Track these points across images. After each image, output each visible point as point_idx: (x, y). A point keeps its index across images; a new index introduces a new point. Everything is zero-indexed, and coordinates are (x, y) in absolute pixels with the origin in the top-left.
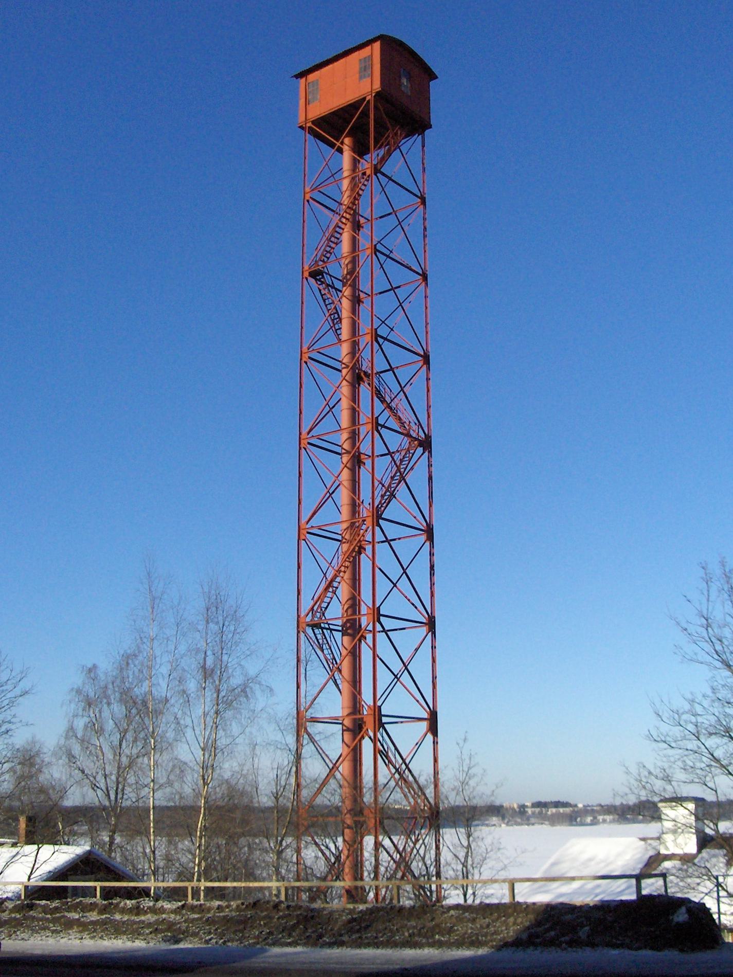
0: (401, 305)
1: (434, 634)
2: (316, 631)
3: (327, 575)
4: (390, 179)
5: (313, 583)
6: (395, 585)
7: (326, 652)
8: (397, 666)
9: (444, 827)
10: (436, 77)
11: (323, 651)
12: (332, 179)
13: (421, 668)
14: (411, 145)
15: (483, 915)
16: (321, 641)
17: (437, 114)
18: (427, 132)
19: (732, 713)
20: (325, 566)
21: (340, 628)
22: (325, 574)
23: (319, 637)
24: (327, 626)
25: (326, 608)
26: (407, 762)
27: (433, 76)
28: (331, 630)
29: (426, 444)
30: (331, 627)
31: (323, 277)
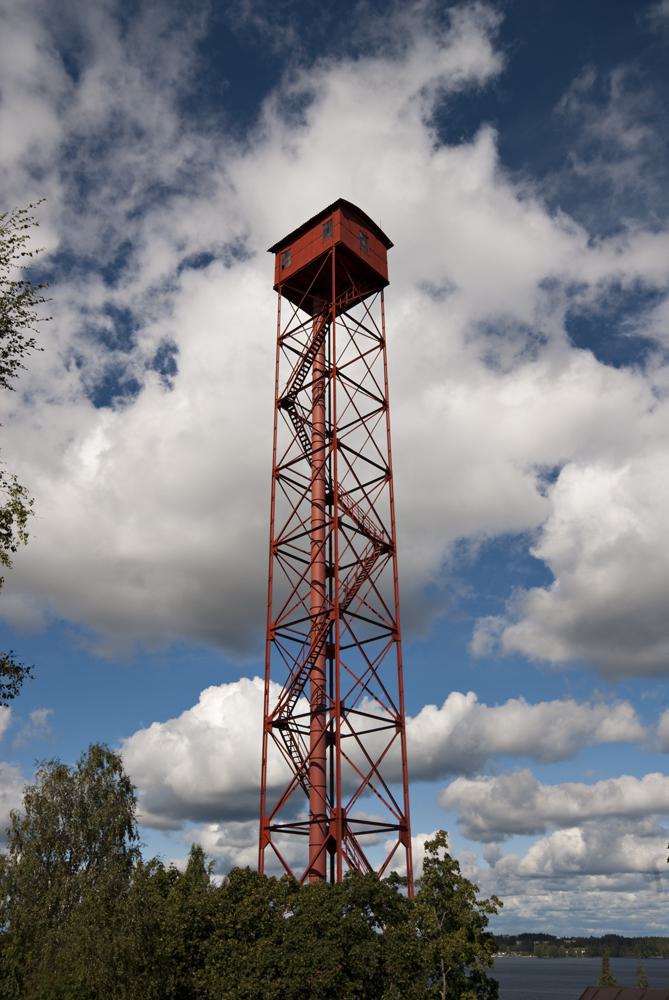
0: (359, 644)
2: (284, 732)
3: (294, 672)
7: (294, 755)
10: (392, 245)
12: (302, 329)
13: (387, 670)
14: (373, 300)
15: (645, 166)
16: (289, 744)
17: (392, 275)
18: (385, 289)
19: (666, 827)
21: (308, 731)
23: (287, 738)
24: (295, 728)
26: (374, 667)
27: (388, 244)
28: (300, 733)
30: (301, 729)
31: (294, 408)
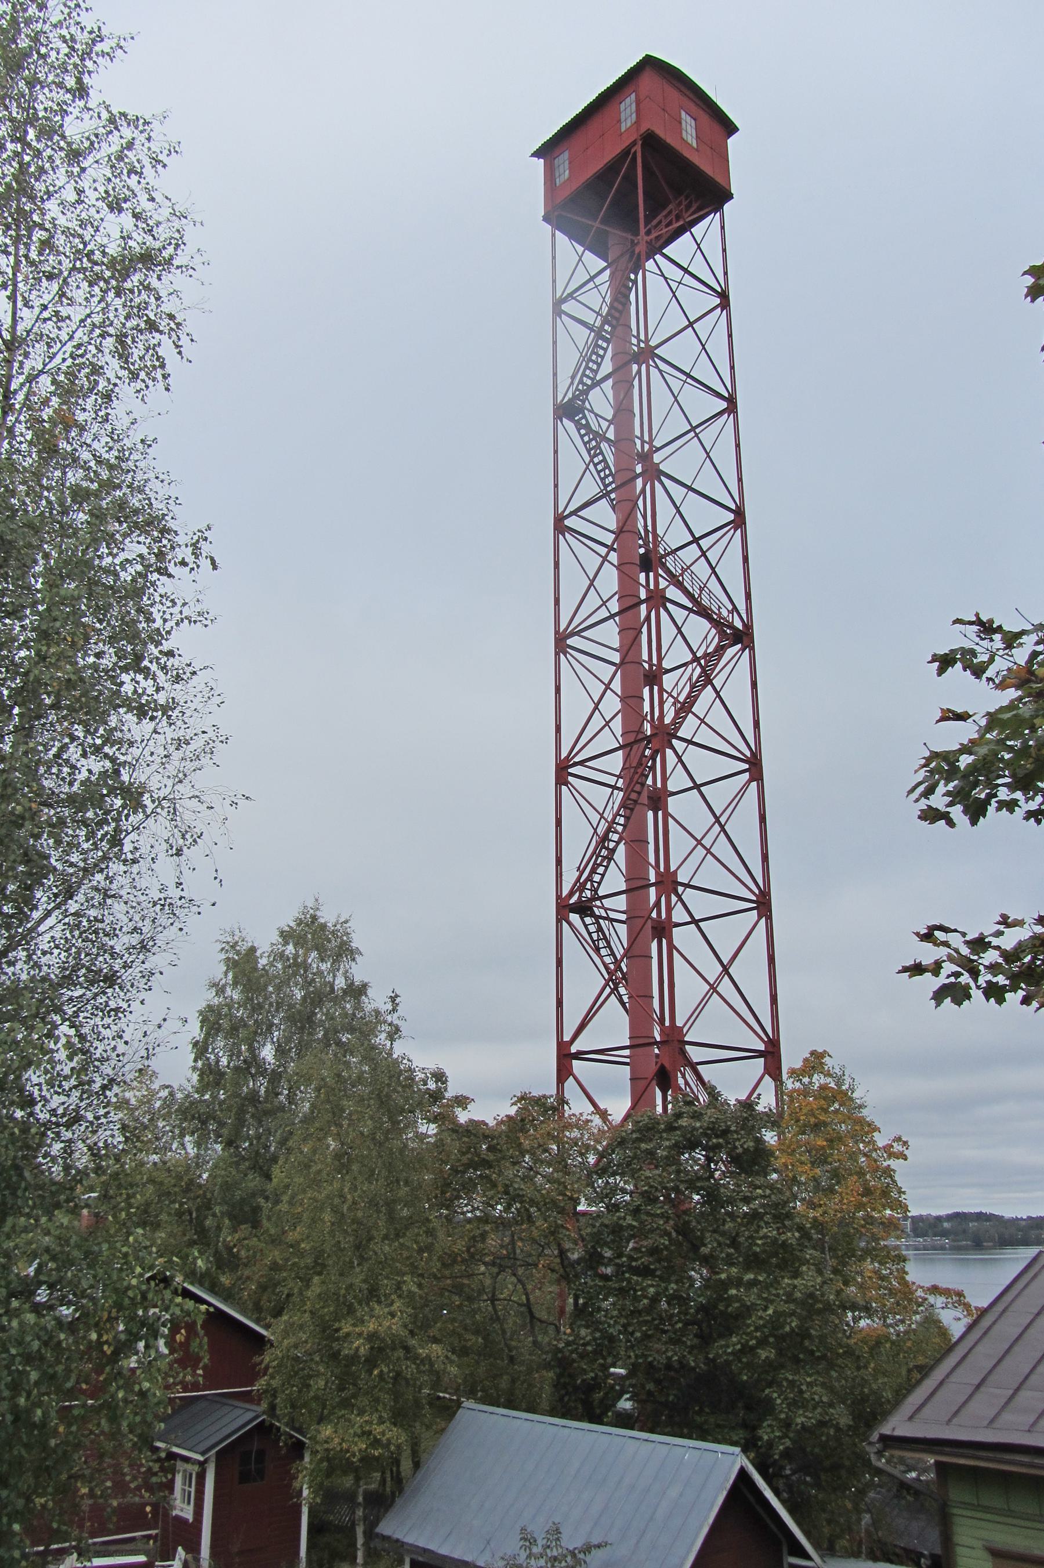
1: (769, 918)
3: (599, 831)
4: (690, 488)
5: (578, 842)
6: (697, 787)
7: (603, 952)
8: (713, 971)
9: (400, 1093)
11: (601, 957)
12: (591, 285)
16: (595, 936)
18: (727, 207)
20: (595, 818)
22: (595, 830)
23: (592, 928)
25: (599, 883)
26: (723, 820)
27: (729, 128)
28: (612, 920)
29: (743, 637)
